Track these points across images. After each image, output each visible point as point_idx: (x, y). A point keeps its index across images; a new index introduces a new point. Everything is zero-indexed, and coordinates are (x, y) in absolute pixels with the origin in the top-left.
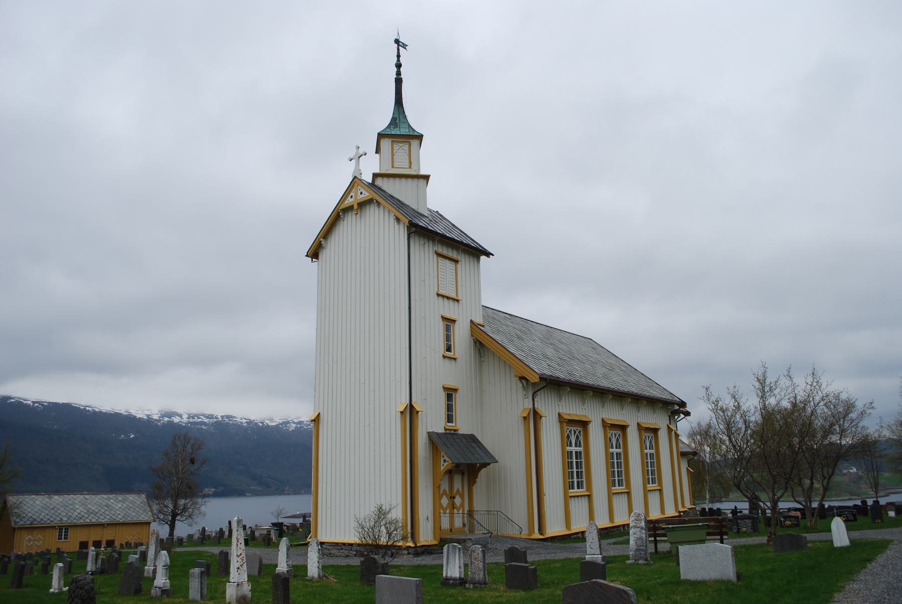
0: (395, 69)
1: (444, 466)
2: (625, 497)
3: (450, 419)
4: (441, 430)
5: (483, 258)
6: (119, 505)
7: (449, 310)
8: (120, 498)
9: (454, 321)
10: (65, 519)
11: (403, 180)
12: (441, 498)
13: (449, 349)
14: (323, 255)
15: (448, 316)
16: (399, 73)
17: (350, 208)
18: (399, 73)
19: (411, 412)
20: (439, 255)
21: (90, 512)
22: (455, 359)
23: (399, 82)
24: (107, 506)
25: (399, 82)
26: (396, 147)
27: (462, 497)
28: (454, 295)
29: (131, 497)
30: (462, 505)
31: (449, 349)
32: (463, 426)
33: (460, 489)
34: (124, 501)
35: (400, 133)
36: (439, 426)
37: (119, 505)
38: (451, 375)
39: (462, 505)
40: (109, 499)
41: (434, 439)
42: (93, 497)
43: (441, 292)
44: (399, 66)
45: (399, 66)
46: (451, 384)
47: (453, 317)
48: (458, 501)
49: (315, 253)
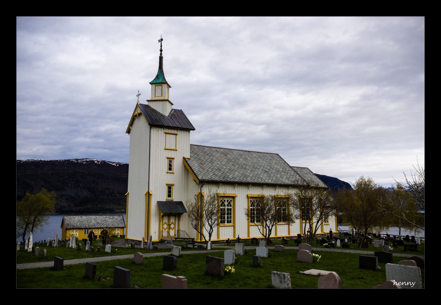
0: (160, 52)
1: (162, 214)
2: (233, 227)
3: (169, 196)
4: (164, 200)
5: (191, 131)
6: (110, 220)
7: (171, 154)
8: (111, 217)
9: (174, 159)
10: (87, 226)
11: (158, 102)
12: (163, 225)
13: (170, 169)
14: (131, 132)
15: (170, 156)
16: (161, 54)
17: (136, 116)
18: (161, 54)
19: (149, 195)
20: (166, 133)
21: (98, 223)
22: (173, 173)
23: (161, 58)
24: (105, 220)
25: (161, 58)
26: (157, 88)
27: (175, 225)
28: (174, 148)
29: (116, 217)
30: (175, 228)
31: (170, 169)
32: (176, 198)
33: (174, 222)
34: (113, 219)
35: (160, 80)
36: (164, 198)
37: (110, 220)
38: (170, 179)
39: (175, 228)
40: (106, 218)
41: (160, 204)
42: (100, 217)
43: (167, 147)
44: (161, 51)
45: (161, 51)
46: (170, 182)
47: (173, 157)
48: (172, 226)
49: (129, 131)
